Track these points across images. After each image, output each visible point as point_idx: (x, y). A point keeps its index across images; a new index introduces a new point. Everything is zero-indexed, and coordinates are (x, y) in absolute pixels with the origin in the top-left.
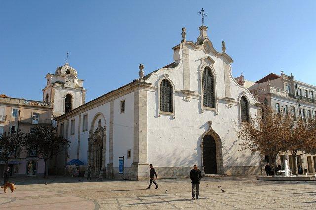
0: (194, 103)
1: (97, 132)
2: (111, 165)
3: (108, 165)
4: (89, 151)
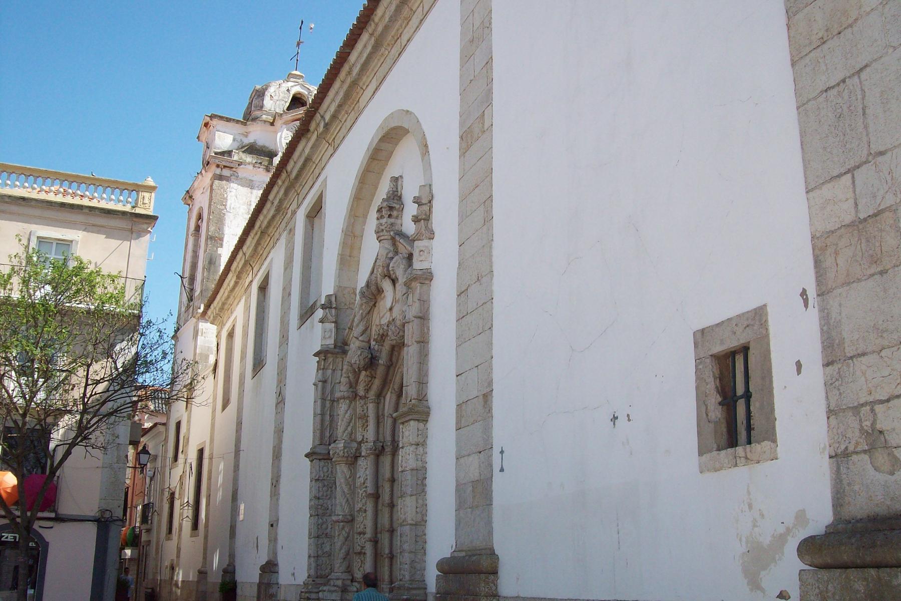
1: (373, 294)
2: (270, 568)
3: (448, 568)
4: (319, 455)
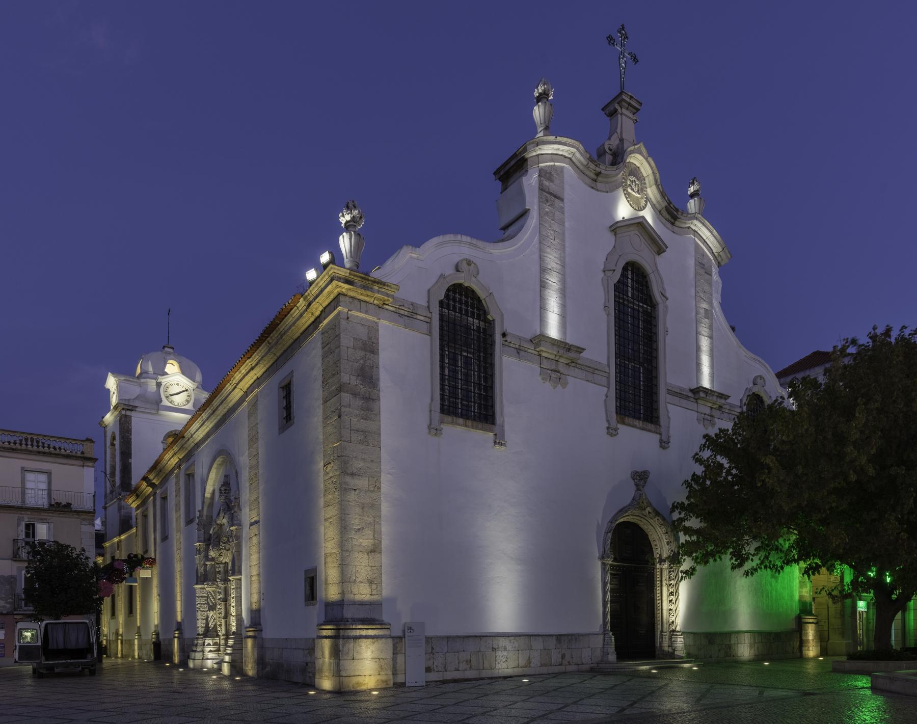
0: (594, 397)
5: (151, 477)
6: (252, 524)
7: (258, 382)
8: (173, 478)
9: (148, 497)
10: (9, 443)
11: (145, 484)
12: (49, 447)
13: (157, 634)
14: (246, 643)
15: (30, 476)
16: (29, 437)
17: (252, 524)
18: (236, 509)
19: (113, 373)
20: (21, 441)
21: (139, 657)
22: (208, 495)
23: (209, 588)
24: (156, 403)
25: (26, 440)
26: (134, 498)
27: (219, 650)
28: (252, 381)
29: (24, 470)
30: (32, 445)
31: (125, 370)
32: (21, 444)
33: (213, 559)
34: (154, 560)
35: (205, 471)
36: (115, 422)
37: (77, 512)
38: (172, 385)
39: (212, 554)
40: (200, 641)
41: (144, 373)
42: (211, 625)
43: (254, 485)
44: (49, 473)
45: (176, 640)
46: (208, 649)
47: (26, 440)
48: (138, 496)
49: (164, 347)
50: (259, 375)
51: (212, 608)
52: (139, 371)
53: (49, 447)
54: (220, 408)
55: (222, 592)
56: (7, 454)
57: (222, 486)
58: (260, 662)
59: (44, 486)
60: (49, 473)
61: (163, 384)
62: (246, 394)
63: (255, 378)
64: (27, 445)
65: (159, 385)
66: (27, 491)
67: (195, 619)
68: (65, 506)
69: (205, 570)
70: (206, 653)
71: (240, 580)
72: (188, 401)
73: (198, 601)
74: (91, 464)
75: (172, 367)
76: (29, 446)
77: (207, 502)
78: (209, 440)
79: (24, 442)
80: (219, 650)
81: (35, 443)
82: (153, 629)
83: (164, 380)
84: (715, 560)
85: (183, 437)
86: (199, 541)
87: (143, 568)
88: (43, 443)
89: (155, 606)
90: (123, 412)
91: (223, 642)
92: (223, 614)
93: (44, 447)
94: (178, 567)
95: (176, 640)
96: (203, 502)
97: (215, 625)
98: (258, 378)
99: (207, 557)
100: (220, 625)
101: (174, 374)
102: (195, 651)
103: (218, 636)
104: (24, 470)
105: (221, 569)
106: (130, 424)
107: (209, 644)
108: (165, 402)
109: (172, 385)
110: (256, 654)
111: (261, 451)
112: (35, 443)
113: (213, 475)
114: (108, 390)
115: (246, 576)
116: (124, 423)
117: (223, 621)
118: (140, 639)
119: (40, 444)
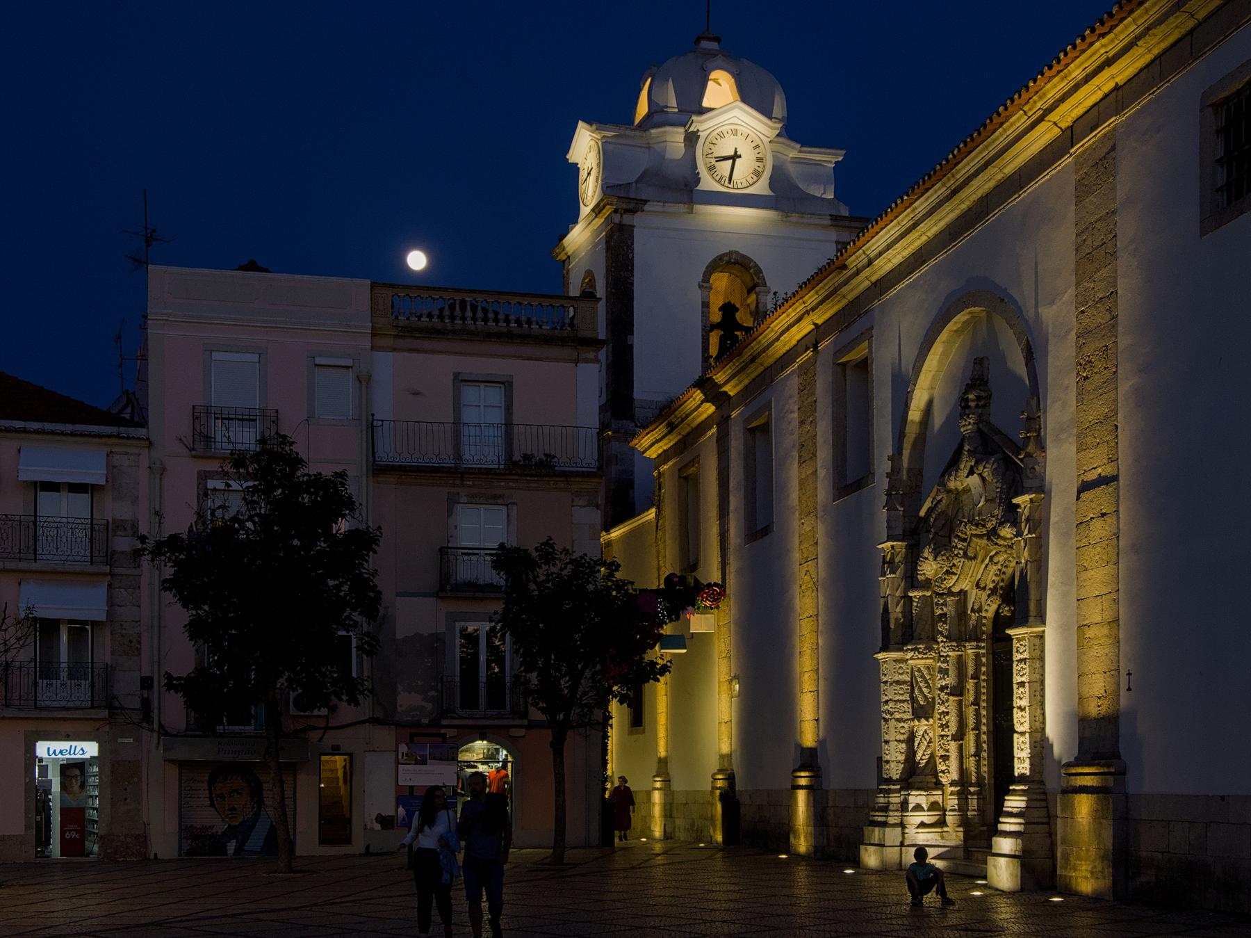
5: (719, 378)
6: (1085, 487)
7: (1118, 98)
8: (791, 378)
9: (703, 427)
10: (430, 316)
11: (698, 395)
12: (507, 321)
13: (731, 778)
14: (1070, 808)
15: (471, 394)
16: (458, 297)
17: (1085, 487)
18: (1031, 448)
19: (589, 122)
20: (441, 310)
21: (667, 836)
22: (914, 415)
23: (916, 660)
24: (684, 187)
25: (452, 307)
26: (660, 430)
27: (941, 823)
28: (1099, 95)
29: (460, 380)
30: (474, 319)
31: (611, 112)
32: (441, 317)
33: (927, 584)
34: (723, 586)
35: (909, 354)
36: (596, 245)
37: (566, 475)
38: (721, 135)
39: (929, 567)
40: (896, 799)
41: (657, 116)
42: (921, 756)
43: (1097, 380)
44: (507, 385)
45: (801, 796)
46: (914, 819)
47: (452, 307)
48: (672, 428)
49: (698, 40)
50: (1121, 79)
51: (922, 712)
52: (642, 108)
53: (507, 321)
54: (975, 183)
55: (952, 672)
56: (426, 344)
57: (969, 388)
58: (1122, 857)
59: (497, 417)
60: (507, 385)
61: (703, 135)
62: (1070, 136)
63: (1111, 85)
64: (463, 319)
65: (692, 139)
66: (466, 430)
67: (876, 741)
68: (541, 464)
69: (907, 612)
70: (911, 830)
71: (1041, 636)
72: (758, 174)
73: (889, 693)
74: (592, 355)
75: (720, 89)
76: (469, 322)
77: (911, 431)
78: (924, 269)
79: (447, 312)
80: (941, 823)
81: (480, 314)
82: (713, 764)
83: (703, 125)
84: (375, 552)
85: (844, 267)
86: (889, 539)
87: (699, 610)
88: (496, 313)
89: (721, 709)
90: (617, 218)
91: (953, 802)
92: (953, 728)
93: (496, 321)
94: (808, 611)
95: (801, 796)
96: (900, 435)
97: (932, 756)
98: (1117, 88)
99: (912, 580)
100: (945, 758)
101: (726, 108)
102: (884, 824)
103: (939, 785)
104: (460, 380)
105: (949, 610)
106: (630, 247)
107: (918, 808)
108: (708, 183)
109: (721, 135)
110: (1108, 834)
111: (1123, 287)
112: (480, 314)
113: (932, 362)
114: (575, 168)
115: (1064, 628)
116: (618, 245)
117: (953, 746)
118: (667, 790)
119: (491, 315)
